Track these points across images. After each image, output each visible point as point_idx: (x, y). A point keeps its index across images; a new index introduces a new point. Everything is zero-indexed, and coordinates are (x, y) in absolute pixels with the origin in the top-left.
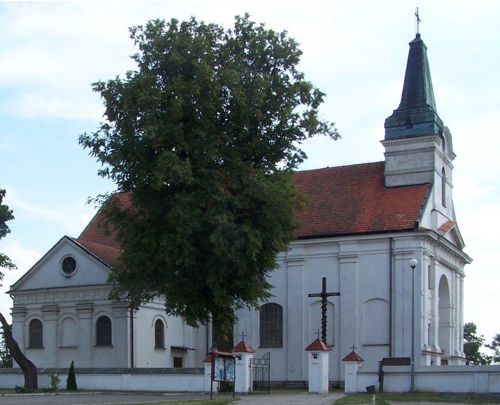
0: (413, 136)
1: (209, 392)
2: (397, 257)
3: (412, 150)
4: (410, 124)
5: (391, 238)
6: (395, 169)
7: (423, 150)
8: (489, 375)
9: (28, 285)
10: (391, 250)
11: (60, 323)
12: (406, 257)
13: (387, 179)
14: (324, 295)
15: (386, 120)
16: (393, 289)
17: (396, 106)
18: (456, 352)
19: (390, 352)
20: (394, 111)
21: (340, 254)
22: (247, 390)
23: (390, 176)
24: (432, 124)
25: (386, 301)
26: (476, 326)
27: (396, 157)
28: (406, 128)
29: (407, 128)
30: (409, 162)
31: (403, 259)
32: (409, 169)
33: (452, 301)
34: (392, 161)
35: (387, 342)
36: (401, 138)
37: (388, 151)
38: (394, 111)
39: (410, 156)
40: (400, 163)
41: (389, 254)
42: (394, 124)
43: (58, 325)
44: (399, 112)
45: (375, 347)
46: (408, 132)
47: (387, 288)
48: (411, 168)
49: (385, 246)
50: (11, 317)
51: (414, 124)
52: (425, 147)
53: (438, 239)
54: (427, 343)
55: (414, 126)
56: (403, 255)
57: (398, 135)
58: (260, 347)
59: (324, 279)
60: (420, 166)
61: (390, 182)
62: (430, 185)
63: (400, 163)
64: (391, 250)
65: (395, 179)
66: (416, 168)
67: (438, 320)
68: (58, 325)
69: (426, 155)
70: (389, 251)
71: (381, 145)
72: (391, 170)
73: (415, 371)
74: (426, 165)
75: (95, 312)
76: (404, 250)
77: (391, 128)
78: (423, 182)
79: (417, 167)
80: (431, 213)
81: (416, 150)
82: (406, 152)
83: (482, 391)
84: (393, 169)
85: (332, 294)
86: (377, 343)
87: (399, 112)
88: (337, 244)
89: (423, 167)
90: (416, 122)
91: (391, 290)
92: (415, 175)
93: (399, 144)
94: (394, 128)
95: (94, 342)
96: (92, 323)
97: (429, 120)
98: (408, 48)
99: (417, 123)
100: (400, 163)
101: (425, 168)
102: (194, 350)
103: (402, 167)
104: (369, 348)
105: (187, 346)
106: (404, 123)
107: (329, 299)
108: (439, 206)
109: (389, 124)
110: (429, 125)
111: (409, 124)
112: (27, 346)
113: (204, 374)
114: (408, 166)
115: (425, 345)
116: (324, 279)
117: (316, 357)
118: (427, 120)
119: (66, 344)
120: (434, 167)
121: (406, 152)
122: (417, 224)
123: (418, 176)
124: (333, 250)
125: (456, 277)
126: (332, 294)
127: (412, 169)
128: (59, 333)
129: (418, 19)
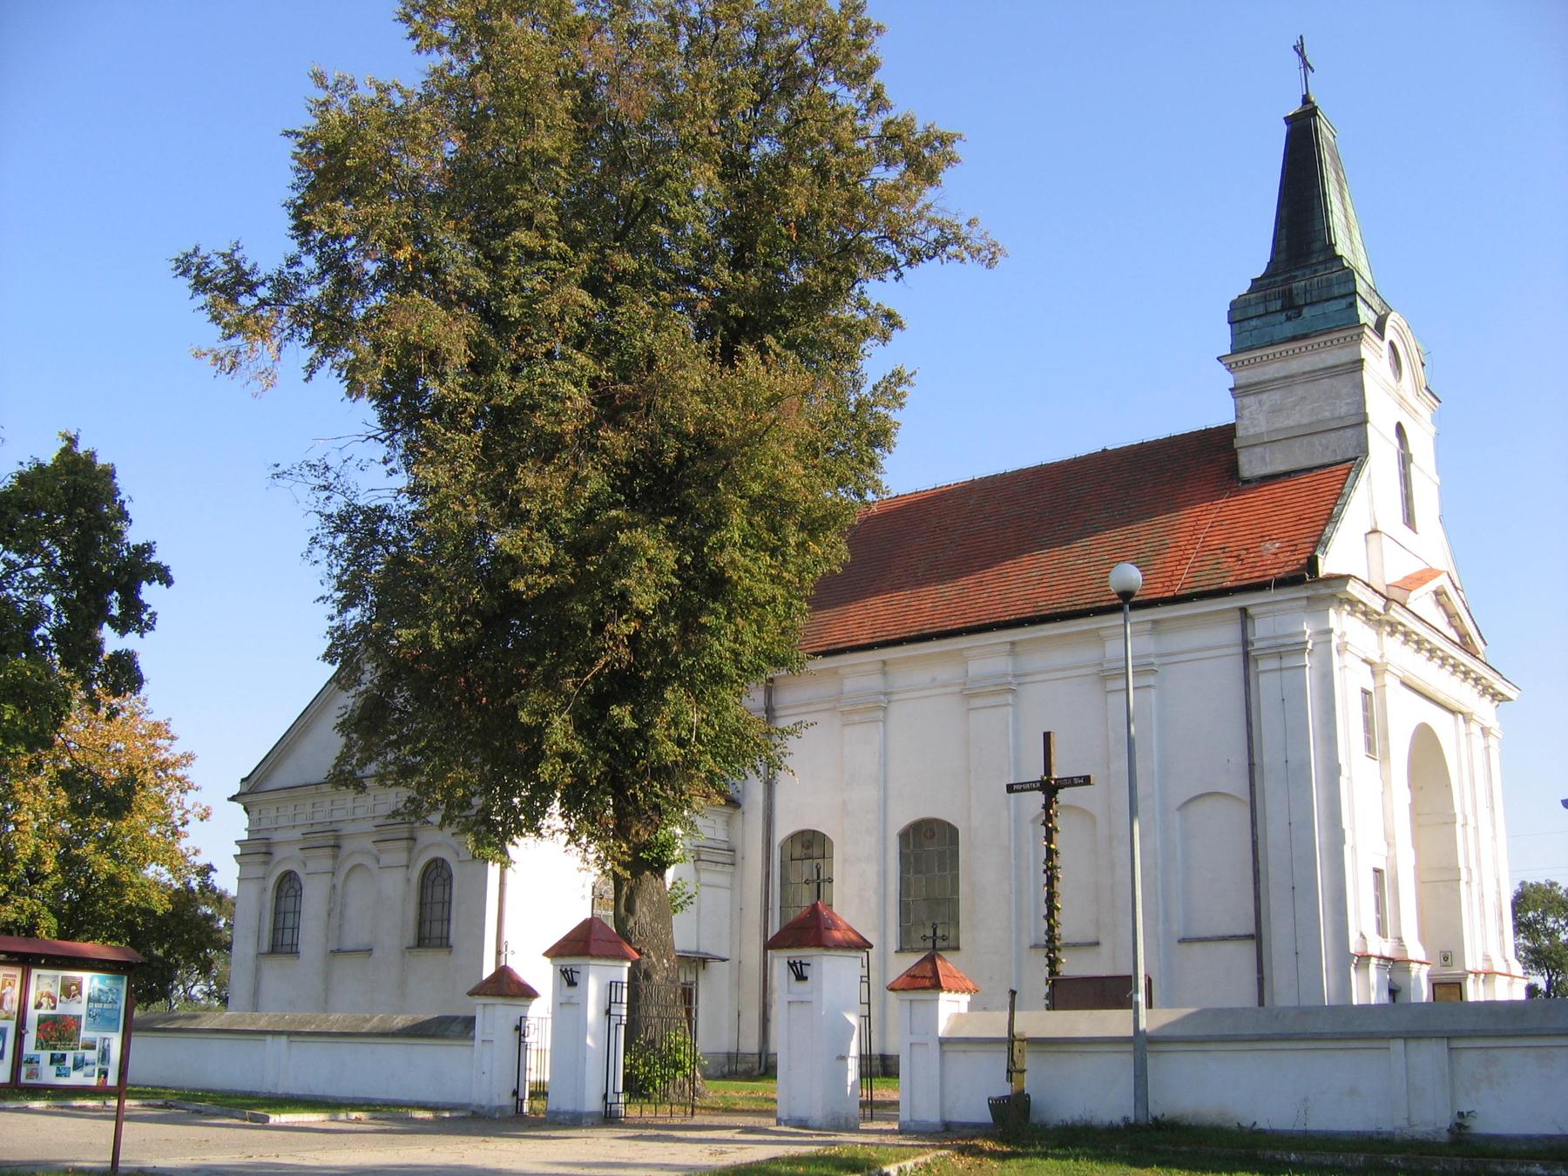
0: (1305, 337)
1: (501, 1108)
2: (1263, 665)
3: (1304, 373)
4: (1291, 308)
5: (1244, 610)
6: (1264, 429)
7: (1331, 371)
8: (1451, 1049)
9: (282, 778)
10: (1246, 643)
11: (340, 880)
12: (1287, 662)
13: (1243, 459)
14: (1049, 788)
15: (1233, 304)
16: (1256, 759)
17: (1259, 270)
18: (1487, 959)
19: (1075, 945)
20: (1253, 280)
21: (1106, 666)
22: (593, 1104)
23: (1251, 450)
24: (1349, 300)
25: (1238, 799)
26: (109, 473)
27: (1265, 396)
28: (1283, 317)
29: (1289, 319)
30: (1298, 408)
31: (1281, 669)
32: (1299, 426)
33: (1463, 805)
34: (1253, 408)
35: (1251, 930)
36: (1272, 344)
37: (1242, 382)
38: (1253, 280)
39: (1300, 390)
40: (1275, 411)
41: (1240, 659)
42: (1251, 312)
43: (334, 887)
44: (1265, 282)
45: (1211, 945)
46: (1289, 329)
47: (1241, 760)
48: (1305, 421)
49: (1229, 633)
50: (236, 869)
51: (1306, 304)
52: (1337, 362)
53: (1386, 608)
54: (1370, 928)
55: (1306, 312)
56: (1280, 656)
57: (1267, 339)
58: (901, 950)
59: (1047, 736)
60: (1328, 414)
61: (1251, 465)
62: (1355, 460)
63: (1275, 411)
64: (1246, 643)
65: (1263, 458)
66: (1319, 422)
67: (1412, 862)
68: (334, 887)
69: (1342, 384)
70: (1240, 650)
71: (1221, 368)
72: (1252, 431)
73: (1007, 1036)
74: (1343, 410)
75: (419, 845)
76: (1280, 641)
77: (1246, 323)
78: (1339, 458)
79: (1320, 417)
80: (1366, 541)
81: (1314, 371)
82: (1288, 381)
83: (1429, 1129)
84: (1258, 430)
85: (1070, 782)
86: (1221, 933)
87: (1265, 282)
88: (1098, 637)
89: (1336, 415)
90: (1308, 301)
91: (1251, 765)
92: (1315, 439)
93: (1262, 361)
94: (1254, 323)
95: (410, 937)
96: (409, 880)
97: (1343, 291)
98: (1283, 129)
99: (1312, 304)
100: (1274, 412)
101: (1341, 418)
102: (724, 960)
103: (1283, 422)
104: (1197, 947)
105: (708, 948)
106: (1278, 305)
107: (1063, 795)
108: (1391, 518)
109: (1239, 314)
110: (1343, 303)
111: (1291, 307)
112: (265, 947)
113: (473, 1038)
114: (1296, 418)
115: (1362, 935)
116: (1047, 736)
117: (801, 977)
118: (1336, 291)
119: (349, 944)
120: (1365, 414)
121: (1288, 381)
122: (1312, 564)
123: (1324, 441)
124: (1086, 654)
125: (1468, 734)
126: (1070, 782)
127: (1311, 424)
128: (336, 910)
129: (1306, 65)
